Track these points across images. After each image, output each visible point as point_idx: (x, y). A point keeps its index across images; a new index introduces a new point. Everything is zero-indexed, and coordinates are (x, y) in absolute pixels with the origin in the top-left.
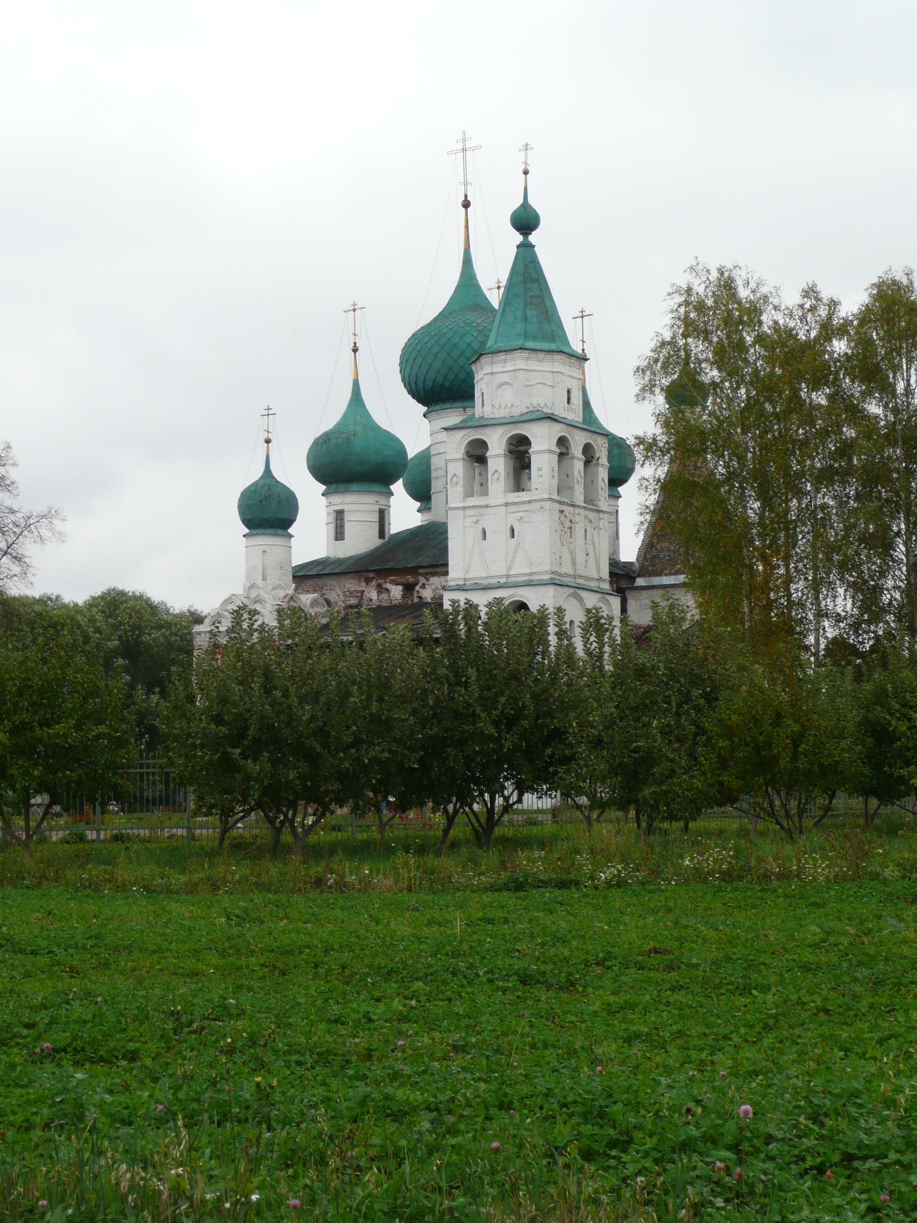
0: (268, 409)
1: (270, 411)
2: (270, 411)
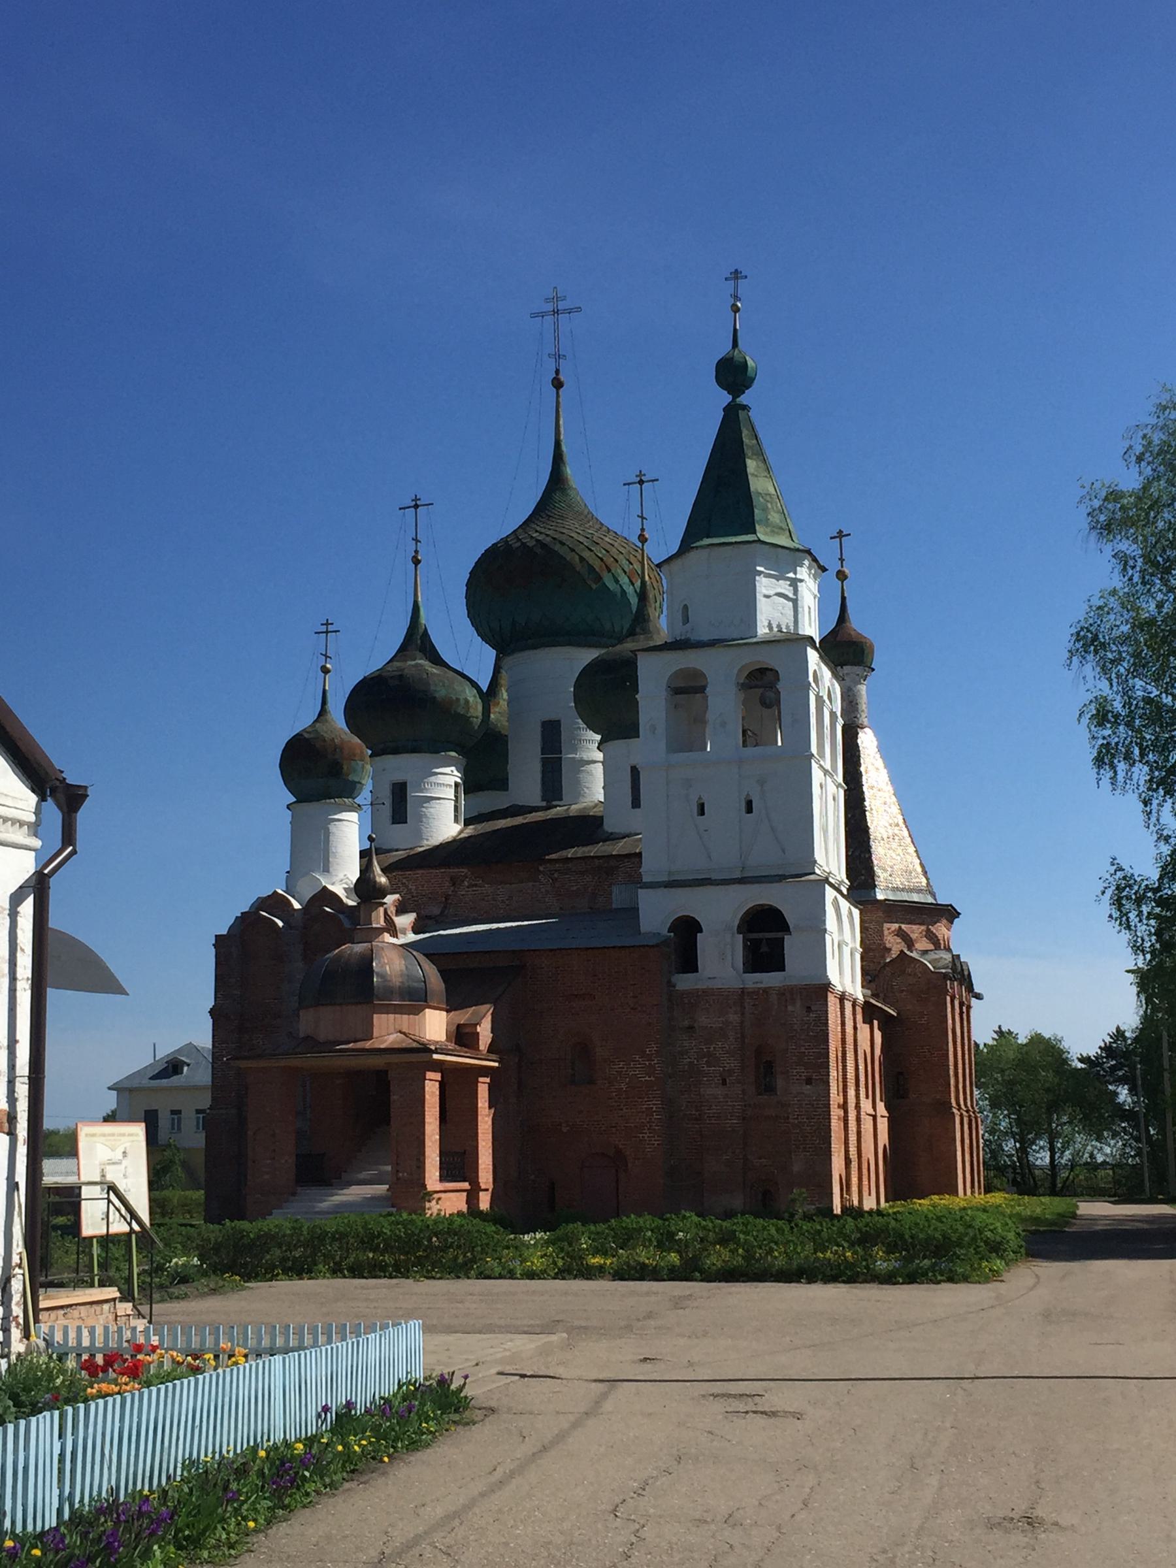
0: (327, 624)
1: (330, 628)
2: (330, 628)
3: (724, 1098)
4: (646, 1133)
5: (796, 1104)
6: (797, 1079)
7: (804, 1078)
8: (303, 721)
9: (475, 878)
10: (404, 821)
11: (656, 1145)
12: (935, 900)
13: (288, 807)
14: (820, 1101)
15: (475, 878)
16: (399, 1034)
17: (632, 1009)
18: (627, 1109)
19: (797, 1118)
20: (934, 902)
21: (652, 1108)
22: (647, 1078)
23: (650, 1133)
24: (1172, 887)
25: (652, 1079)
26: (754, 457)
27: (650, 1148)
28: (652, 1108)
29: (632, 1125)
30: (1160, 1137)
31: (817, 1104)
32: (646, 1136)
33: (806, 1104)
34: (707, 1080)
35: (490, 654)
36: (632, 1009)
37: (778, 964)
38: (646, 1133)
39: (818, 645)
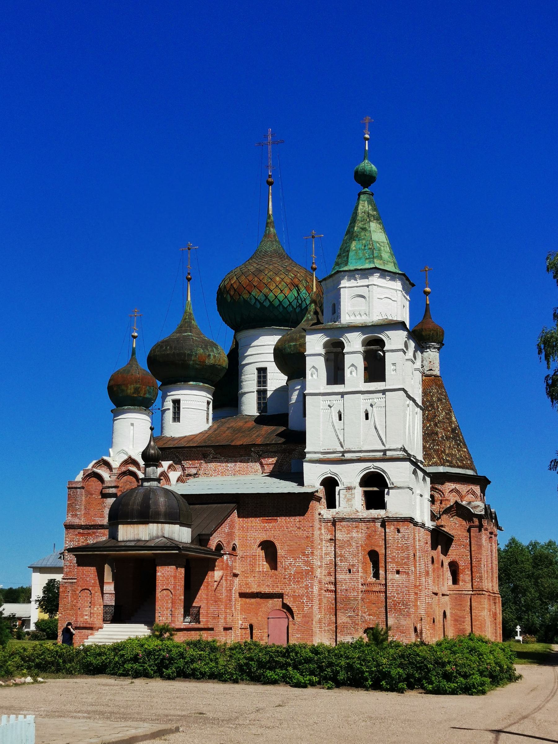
3: (349, 581)
4: (305, 599)
5: (391, 585)
6: (391, 571)
7: (395, 570)
8: (122, 364)
9: (216, 453)
10: (179, 420)
11: (310, 606)
12: (477, 473)
13: (112, 411)
14: (404, 584)
15: (216, 453)
16: (163, 538)
17: (299, 528)
18: (294, 585)
19: (391, 594)
20: (475, 474)
21: (308, 585)
22: (306, 568)
23: (307, 599)
24: (449, 651)
25: (308, 568)
26: (375, 221)
27: (307, 608)
28: (308, 585)
29: (297, 594)
30: (367, 119)
31: (402, 586)
32: (305, 601)
33: (396, 586)
34: (340, 570)
35: (232, 332)
36: (299, 528)
37: (382, 505)
38: (305, 599)
39: (408, 326)
